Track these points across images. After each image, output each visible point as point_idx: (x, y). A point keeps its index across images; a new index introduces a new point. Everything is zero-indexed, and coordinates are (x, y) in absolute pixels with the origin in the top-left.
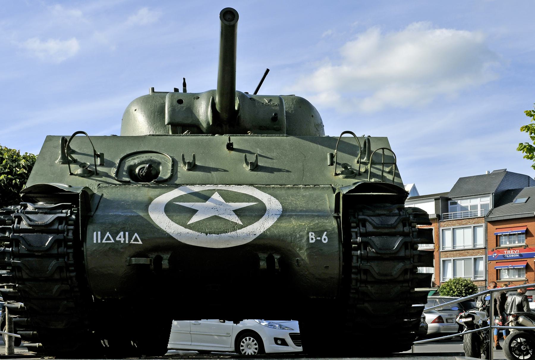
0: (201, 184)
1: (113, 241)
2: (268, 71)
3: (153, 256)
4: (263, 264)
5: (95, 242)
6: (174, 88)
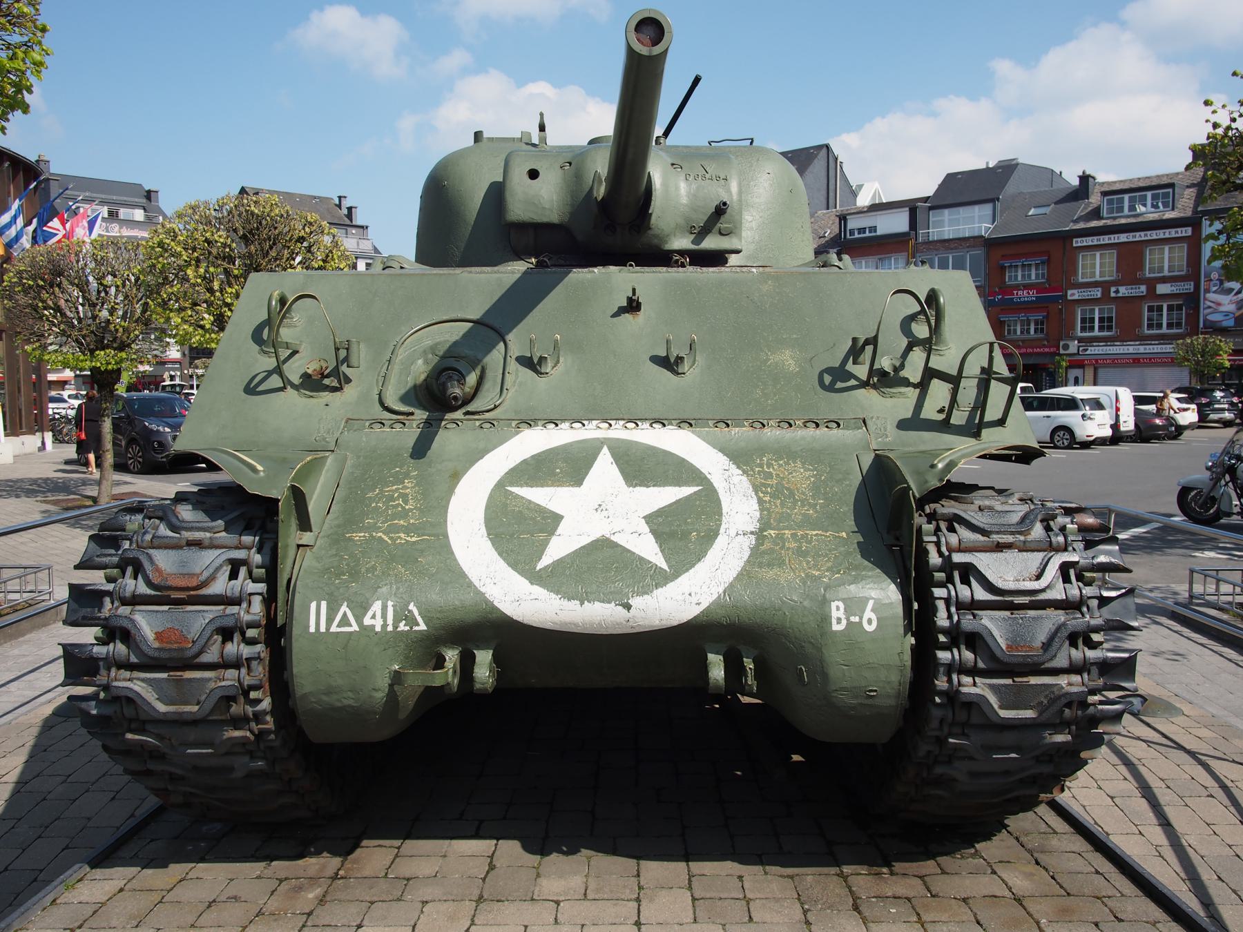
1: (355, 627)
2: (697, 80)
6: (649, 519)
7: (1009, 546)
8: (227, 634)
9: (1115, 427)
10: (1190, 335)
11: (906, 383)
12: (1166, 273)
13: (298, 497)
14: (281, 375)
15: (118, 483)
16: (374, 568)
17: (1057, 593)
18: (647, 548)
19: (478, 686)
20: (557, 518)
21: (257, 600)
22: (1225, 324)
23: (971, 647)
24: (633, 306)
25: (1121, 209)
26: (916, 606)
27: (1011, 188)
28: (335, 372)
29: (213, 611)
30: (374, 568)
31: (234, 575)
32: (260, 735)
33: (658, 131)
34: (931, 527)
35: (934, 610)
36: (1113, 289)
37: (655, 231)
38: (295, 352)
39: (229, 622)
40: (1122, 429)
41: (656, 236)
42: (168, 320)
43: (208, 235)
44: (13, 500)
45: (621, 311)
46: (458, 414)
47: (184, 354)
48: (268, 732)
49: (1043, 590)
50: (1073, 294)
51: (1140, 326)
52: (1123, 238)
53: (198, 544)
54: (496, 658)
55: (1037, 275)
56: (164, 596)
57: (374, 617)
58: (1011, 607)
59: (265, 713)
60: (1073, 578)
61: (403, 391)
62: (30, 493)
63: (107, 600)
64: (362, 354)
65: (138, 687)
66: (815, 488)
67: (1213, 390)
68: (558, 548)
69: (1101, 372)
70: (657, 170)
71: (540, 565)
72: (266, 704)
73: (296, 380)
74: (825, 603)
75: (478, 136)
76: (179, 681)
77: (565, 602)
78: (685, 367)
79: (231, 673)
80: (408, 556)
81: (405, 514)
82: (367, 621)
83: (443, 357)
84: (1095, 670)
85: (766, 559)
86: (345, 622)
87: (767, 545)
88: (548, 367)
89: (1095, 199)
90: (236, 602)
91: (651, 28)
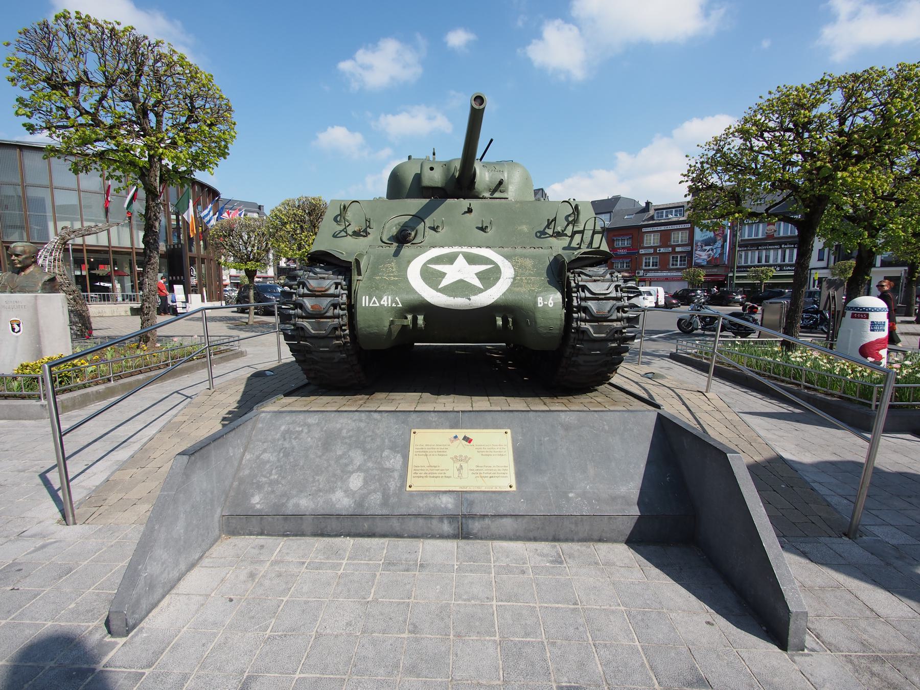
1: (378, 305)
2: (492, 140)
5: (364, 305)
6: (476, 274)
7: (599, 280)
8: (335, 306)
9: (656, 303)
10: (689, 268)
11: (566, 235)
12: (680, 243)
13: (358, 262)
14: (346, 232)
15: (255, 318)
16: (383, 287)
17: (614, 295)
18: (477, 282)
19: (419, 326)
20: (445, 274)
21: (344, 296)
22: (703, 264)
23: (584, 312)
24: (470, 211)
25: (662, 216)
26: (566, 300)
27: (617, 207)
28: (365, 231)
29: (329, 299)
30: (383, 287)
31: (336, 288)
32: (345, 343)
33: (478, 156)
34: (573, 275)
35: (573, 300)
36: (658, 249)
37: (476, 190)
38: (350, 224)
39: (336, 302)
40: (659, 304)
41: (477, 192)
42: (279, 246)
43: (295, 211)
44: (214, 323)
45: (465, 212)
46: (409, 244)
47: (275, 274)
48: (348, 342)
49: (609, 294)
50: (642, 251)
51: (669, 265)
52: (663, 228)
53: (324, 278)
54: (425, 319)
55: (627, 243)
56: (313, 294)
58: (598, 299)
59: (347, 334)
60: (619, 290)
61: (388, 237)
62: (220, 321)
63: (294, 295)
64: (373, 224)
65: (305, 324)
66: (534, 266)
67: (697, 290)
68: (445, 282)
69: (652, 283)
70: (478, 166)
71: (440, 287)
72: (347, 332)
73: (350, 233)
74: (536, 297)
75: (410, 157)
76: (319, 322)
77: (449, 298)
78: (488, 230)
79: (336, 320)
80: (395, 283)
81: (393, 272)
82: (382, 303)
83: (402, 227)
84: (625, 320)
85: (516, 285)
86: (374, 303)
87: (517, 281)
88: (440, 230)
89: (652, 212)
90: (338, 296)
91: (479, 99)
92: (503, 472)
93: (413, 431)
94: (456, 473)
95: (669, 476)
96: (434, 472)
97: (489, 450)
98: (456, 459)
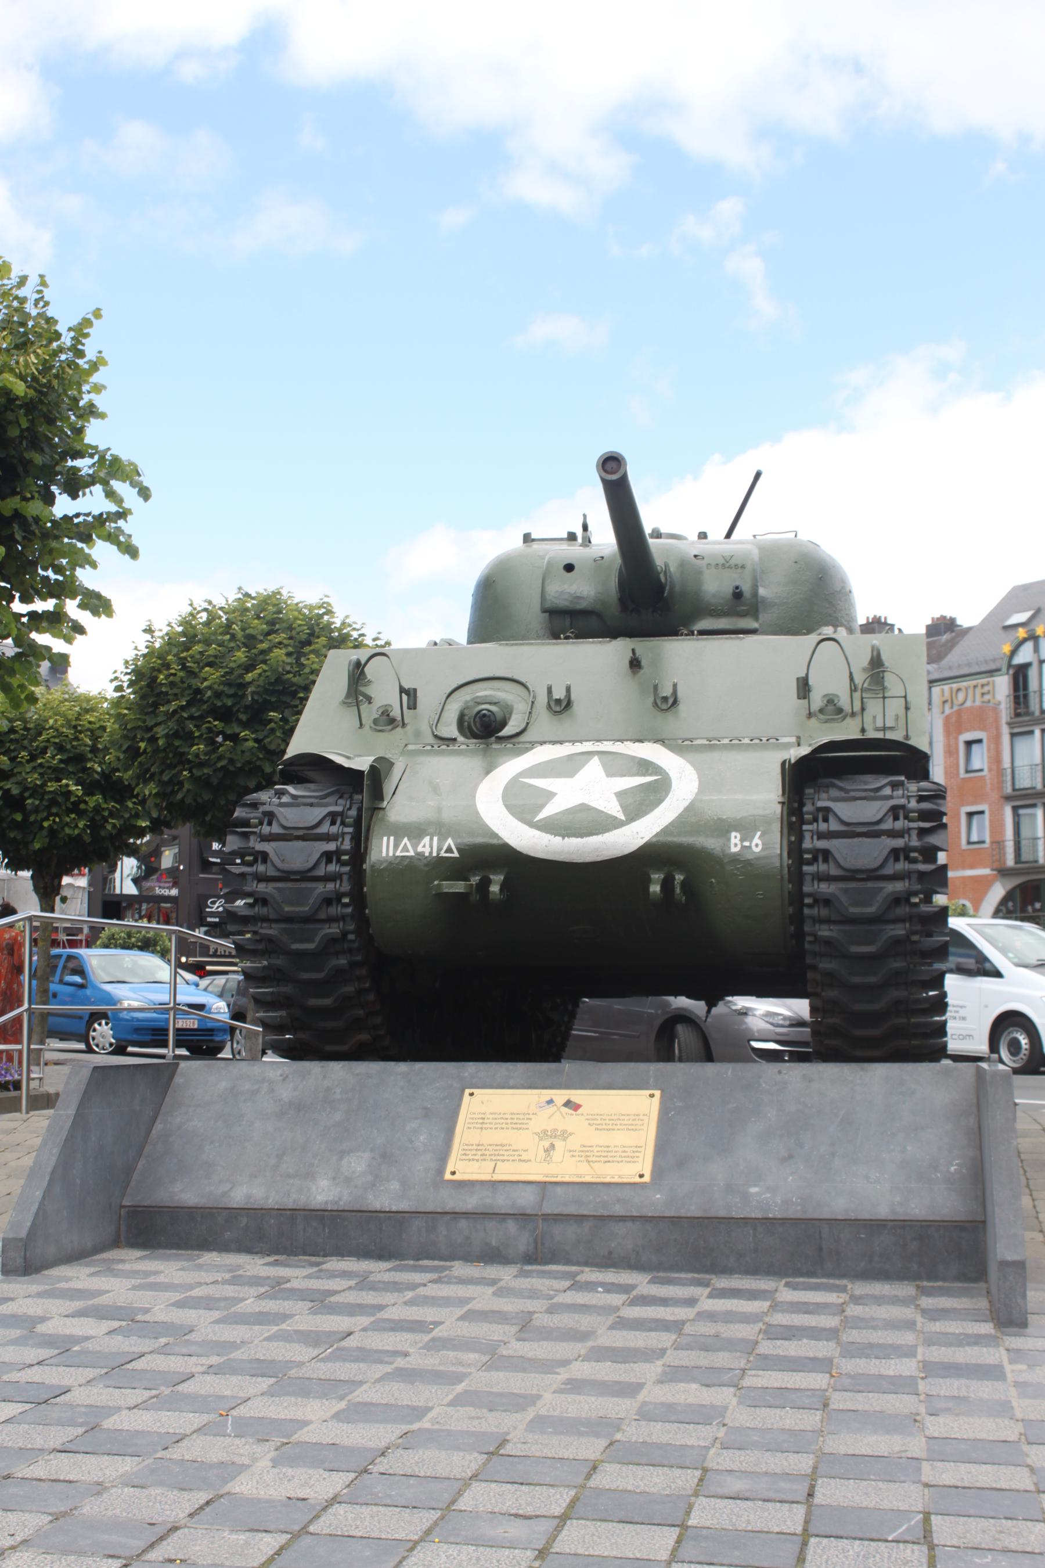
0: (573, 742)
1: (412, 853)
2: (758, 475)
3: (475, 880)
4: (655, 888)
5: (384, 854)
17: (888, 825)
21: (347, 838)
23: (826, 860)
57: (424, 846)
79: (330, 886)
82: (420, 849)
84: (914, 877)
92: (632, 1154)
93: (467, 1091)
94: (542, 1154)
95: (957, 1164)
96: (501, 1153)
97: (611, 1122)
98: (544, 1134)
